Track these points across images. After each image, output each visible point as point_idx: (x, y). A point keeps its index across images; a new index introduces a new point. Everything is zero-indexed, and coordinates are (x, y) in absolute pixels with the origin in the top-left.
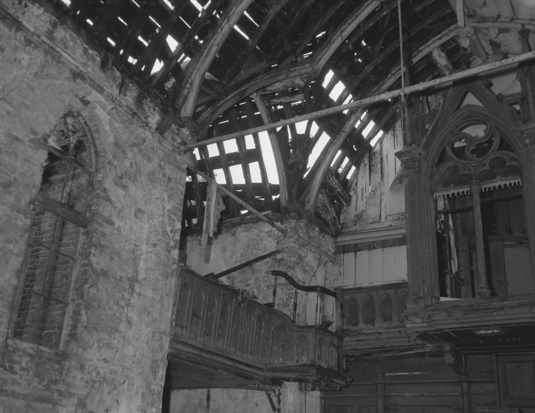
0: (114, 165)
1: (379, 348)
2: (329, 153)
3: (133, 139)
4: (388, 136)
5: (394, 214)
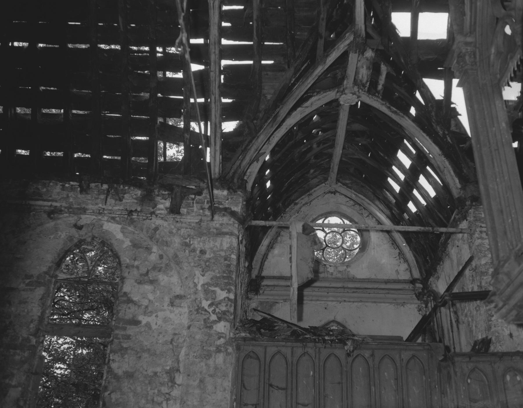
0: (135, 266)
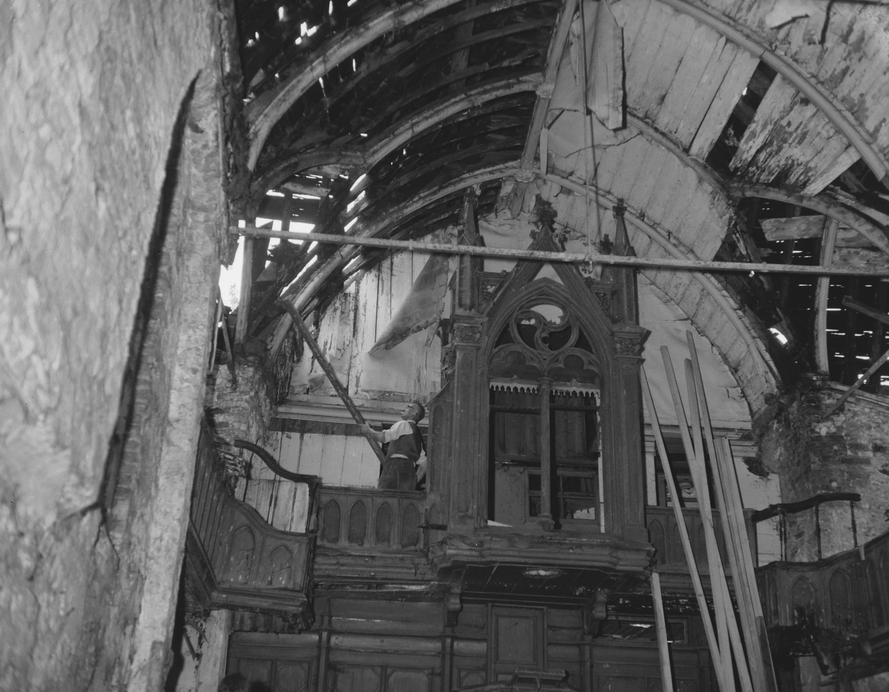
1: (367, 578)
2: (312, 280)
3: (207, 199)
4: (369, 276)
5: (373, 391)
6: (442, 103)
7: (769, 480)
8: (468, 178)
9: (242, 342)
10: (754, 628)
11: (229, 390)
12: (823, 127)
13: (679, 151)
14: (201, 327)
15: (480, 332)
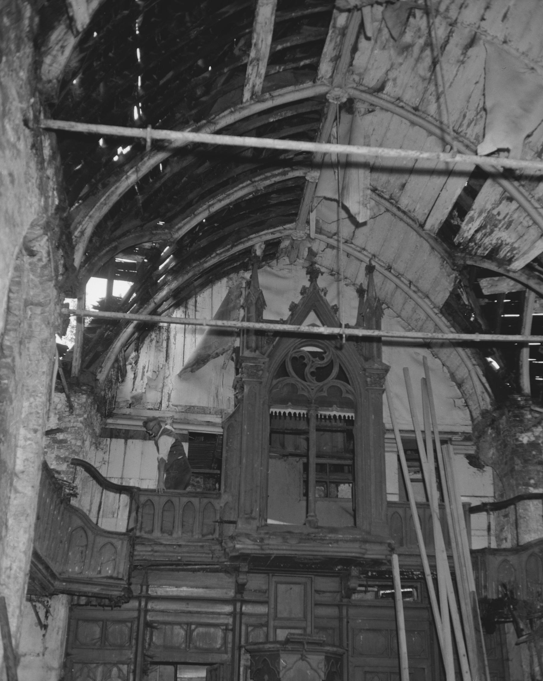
3: (43, 297)
5: (180, 406)
6: (232, 188)
7: (484, 471)
8: (255, 237)
9: (77, 376)
10: (468, 601)
11: (67, 414)
12: (524, 218)
13: (416, 226)
14: (40, 395)
15: (262, 370)
